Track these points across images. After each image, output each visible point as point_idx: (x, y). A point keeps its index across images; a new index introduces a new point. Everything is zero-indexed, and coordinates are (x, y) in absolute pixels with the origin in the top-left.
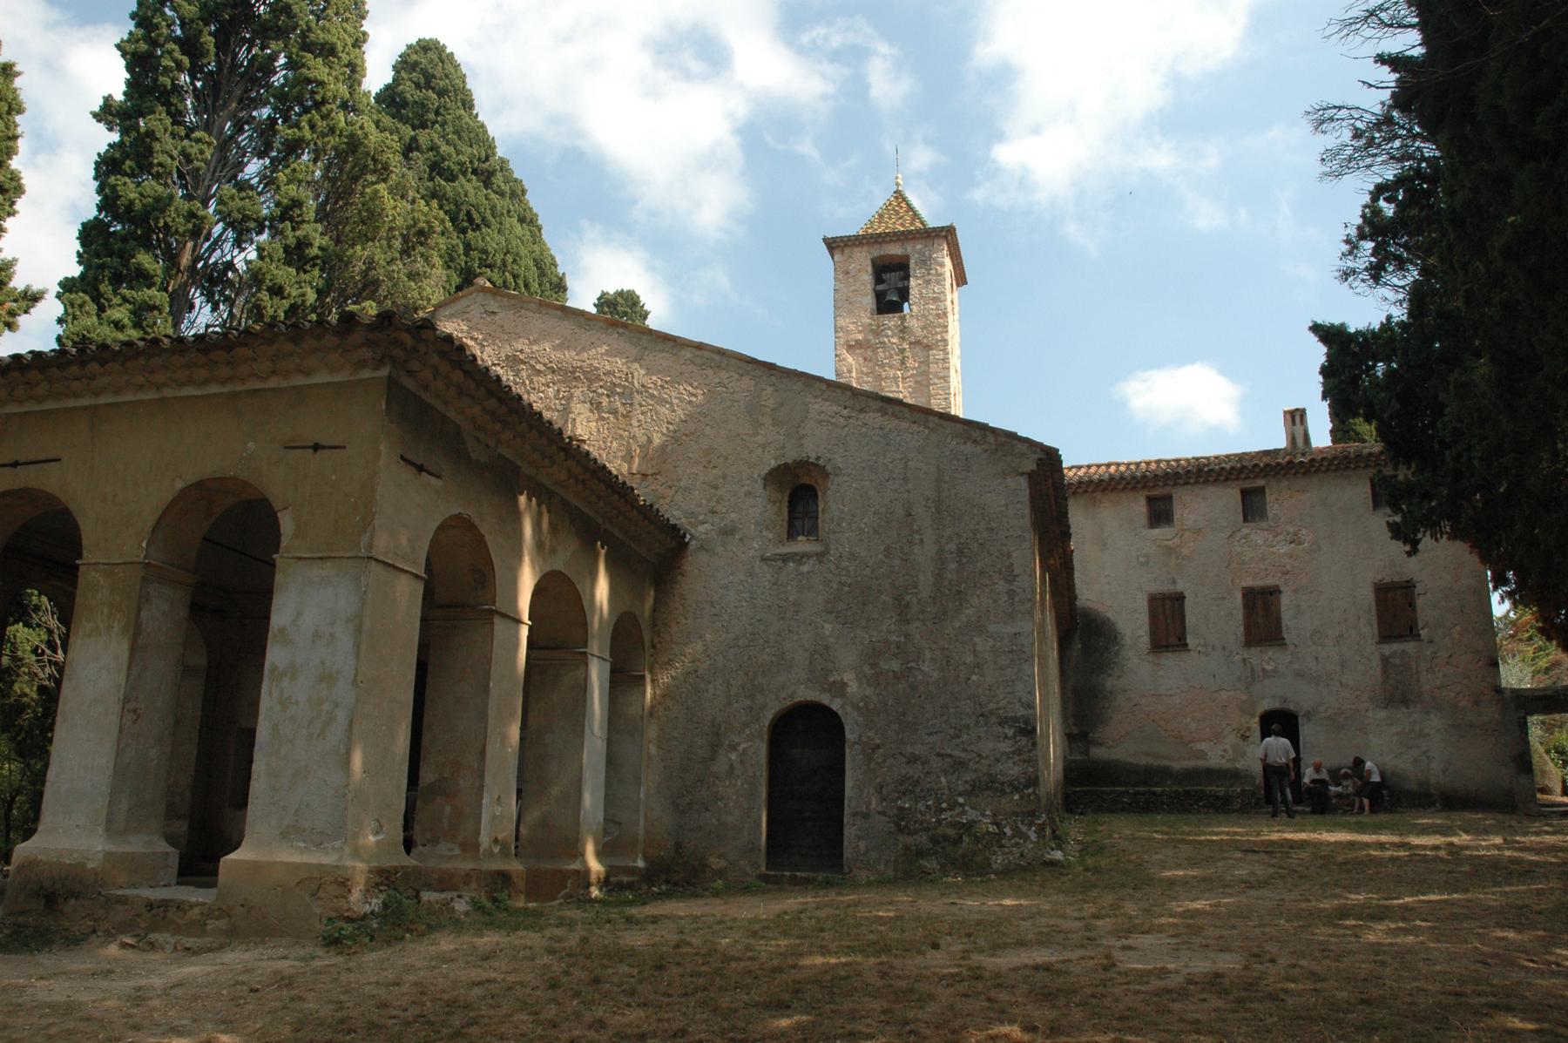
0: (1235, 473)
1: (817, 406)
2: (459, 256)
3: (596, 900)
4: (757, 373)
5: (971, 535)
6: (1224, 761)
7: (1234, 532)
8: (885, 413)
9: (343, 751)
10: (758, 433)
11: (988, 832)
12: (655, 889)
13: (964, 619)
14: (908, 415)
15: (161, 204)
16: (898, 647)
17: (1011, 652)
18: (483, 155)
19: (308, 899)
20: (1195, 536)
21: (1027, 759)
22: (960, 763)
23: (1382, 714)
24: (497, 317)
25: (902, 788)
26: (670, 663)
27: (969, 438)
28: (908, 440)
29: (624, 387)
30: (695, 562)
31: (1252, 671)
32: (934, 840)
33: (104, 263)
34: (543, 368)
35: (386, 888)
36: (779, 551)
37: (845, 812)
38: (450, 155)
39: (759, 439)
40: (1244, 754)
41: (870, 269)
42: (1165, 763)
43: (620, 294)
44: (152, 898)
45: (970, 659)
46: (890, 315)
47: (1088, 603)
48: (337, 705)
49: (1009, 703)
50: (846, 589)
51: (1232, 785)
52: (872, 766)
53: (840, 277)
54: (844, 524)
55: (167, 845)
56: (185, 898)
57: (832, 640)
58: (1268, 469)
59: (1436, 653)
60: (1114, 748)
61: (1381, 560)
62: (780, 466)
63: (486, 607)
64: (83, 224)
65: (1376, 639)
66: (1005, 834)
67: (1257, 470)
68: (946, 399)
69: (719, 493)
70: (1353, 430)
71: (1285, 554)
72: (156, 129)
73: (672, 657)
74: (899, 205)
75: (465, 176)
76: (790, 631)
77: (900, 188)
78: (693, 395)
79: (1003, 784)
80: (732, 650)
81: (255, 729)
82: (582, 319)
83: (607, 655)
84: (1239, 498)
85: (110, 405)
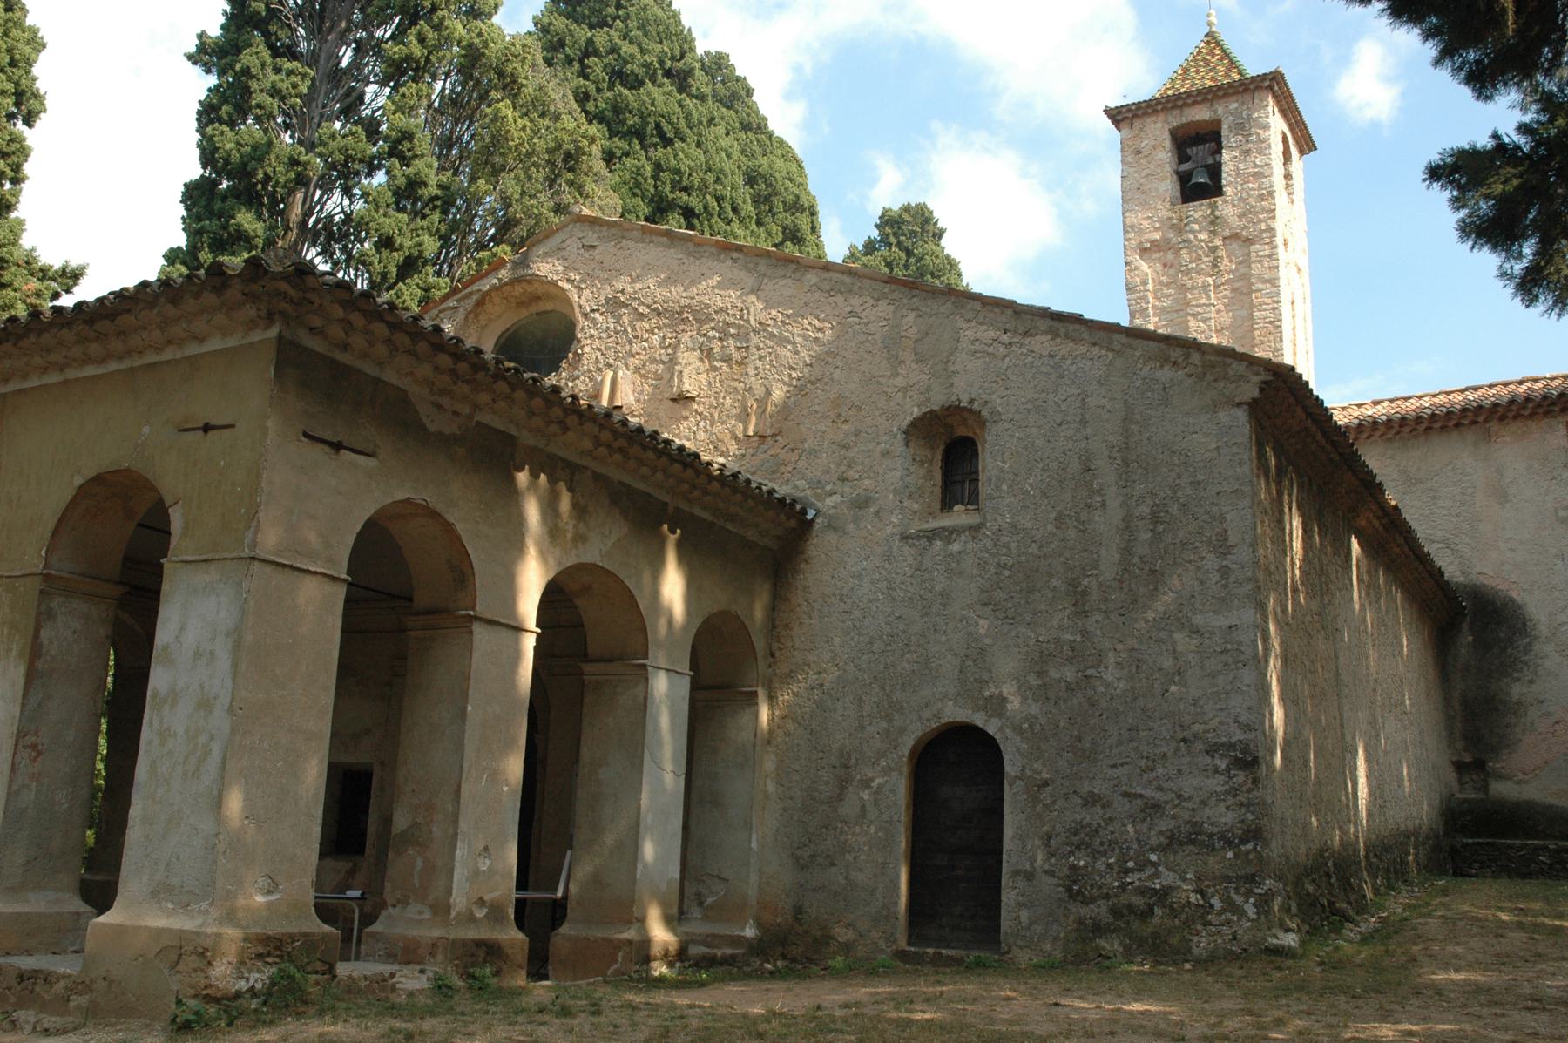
1: (969, 333)
2: (645, 180)
3: (661, 980)
4: (896, 295)
9: (215, 792)
12: (768, 966)
13: (1161, 609)
14: (1085, 335)
15: (260, 152)
16: (1073, 649)
18: (678, 52)
19: (166, 972)
21: (1246, 802)
24: (594, 253)
25: (1076, 840)
26: (790, 676)
27: (1167, 360)
28: (1087, 369)
29: (739, 327)
30: (820, 545)
32: (1116, 912)
33: (202, 227)
34: (647, 311)
35: (277, 960)
36: (926, 526)
37: (1004, 871)
38: (633, 56)
39: (899, 381)
41: (1168, 144)
43: (907, 209)
44: (23, 967)
45: (1167, 663)
47: (1481, 578)
48: (212, 738)
50: (1007, 573)
52: (1039, 808)
53: (1129, 159)
54: (1004, 487)
55: (82, 903)
56: (52, 969)
57: (988, 641)
60: (1526, 782)
62: (925, 414)
63: (464, 612)
64: (185, 185)
66: (1212, 906)
69: (851, 454)
72: (251, 65)
73: (794, 667)
75: (654, 82)
76: (935, 630)
77: (1214, 29)
78: (819, 330)
79: (1211, 836)
80: (865, 657)
82: (690, 245)
83: (685, 667)
85: (19, 392)
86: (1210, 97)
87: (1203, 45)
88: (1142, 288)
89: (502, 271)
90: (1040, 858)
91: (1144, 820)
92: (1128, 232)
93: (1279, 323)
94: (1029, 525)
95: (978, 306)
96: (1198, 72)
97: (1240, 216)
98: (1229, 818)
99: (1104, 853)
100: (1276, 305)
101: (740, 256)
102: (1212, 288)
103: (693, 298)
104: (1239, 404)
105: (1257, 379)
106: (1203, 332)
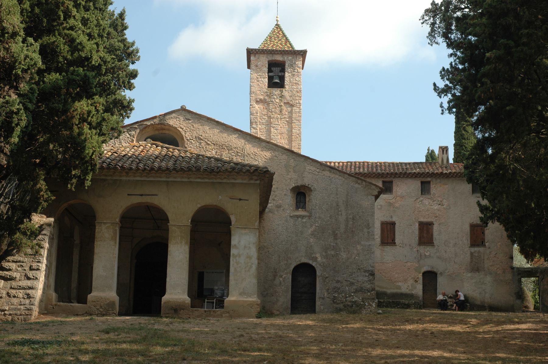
0: (419, 175)
1: (308, 167)
4: (288, 154)
5: (357, 213)
6: (407, 290)
7: (417, 199)
8: (331, 172)
10: (289, 175)
11: (361, 304)
16: (334, 247)
20: (401, 199)
22: (352, 283)
23: (469, 275)
27: (357, 182)
29: (242, 154)
31: (421, 255)
32: (345, 306)
39: (289, 176)
40: (416, 288)
42: (385, 290)
45: (355, 252)
46: (276, 89)
48: (253, 264)
49: (367, 266)
52: (325, 283)
54: (317, 207)
57: (313, 244)
58: (432, 174)
59: (491, 252)
61: (473, 215)
65: (469, 246)
67: (428, 174)
68: (299, 130)
70: (464, 146)
71: (436, 209)
77: (279, 23)
79: (365, 290)
82: (224, 126)
84: (420, 185)
86: (283, 53)
87: (275, 28)
88: (256, 114)
89: (155, 120)
91: (350, 286)
92: (252, 94)
93: (300, 135)
94: (323, 217)
95: (311, 161)
96: (275, 40)
98: (369, 286)
102: (279, 119)
103: (226, 142)
104: (373, 195)
105: (377, 190)
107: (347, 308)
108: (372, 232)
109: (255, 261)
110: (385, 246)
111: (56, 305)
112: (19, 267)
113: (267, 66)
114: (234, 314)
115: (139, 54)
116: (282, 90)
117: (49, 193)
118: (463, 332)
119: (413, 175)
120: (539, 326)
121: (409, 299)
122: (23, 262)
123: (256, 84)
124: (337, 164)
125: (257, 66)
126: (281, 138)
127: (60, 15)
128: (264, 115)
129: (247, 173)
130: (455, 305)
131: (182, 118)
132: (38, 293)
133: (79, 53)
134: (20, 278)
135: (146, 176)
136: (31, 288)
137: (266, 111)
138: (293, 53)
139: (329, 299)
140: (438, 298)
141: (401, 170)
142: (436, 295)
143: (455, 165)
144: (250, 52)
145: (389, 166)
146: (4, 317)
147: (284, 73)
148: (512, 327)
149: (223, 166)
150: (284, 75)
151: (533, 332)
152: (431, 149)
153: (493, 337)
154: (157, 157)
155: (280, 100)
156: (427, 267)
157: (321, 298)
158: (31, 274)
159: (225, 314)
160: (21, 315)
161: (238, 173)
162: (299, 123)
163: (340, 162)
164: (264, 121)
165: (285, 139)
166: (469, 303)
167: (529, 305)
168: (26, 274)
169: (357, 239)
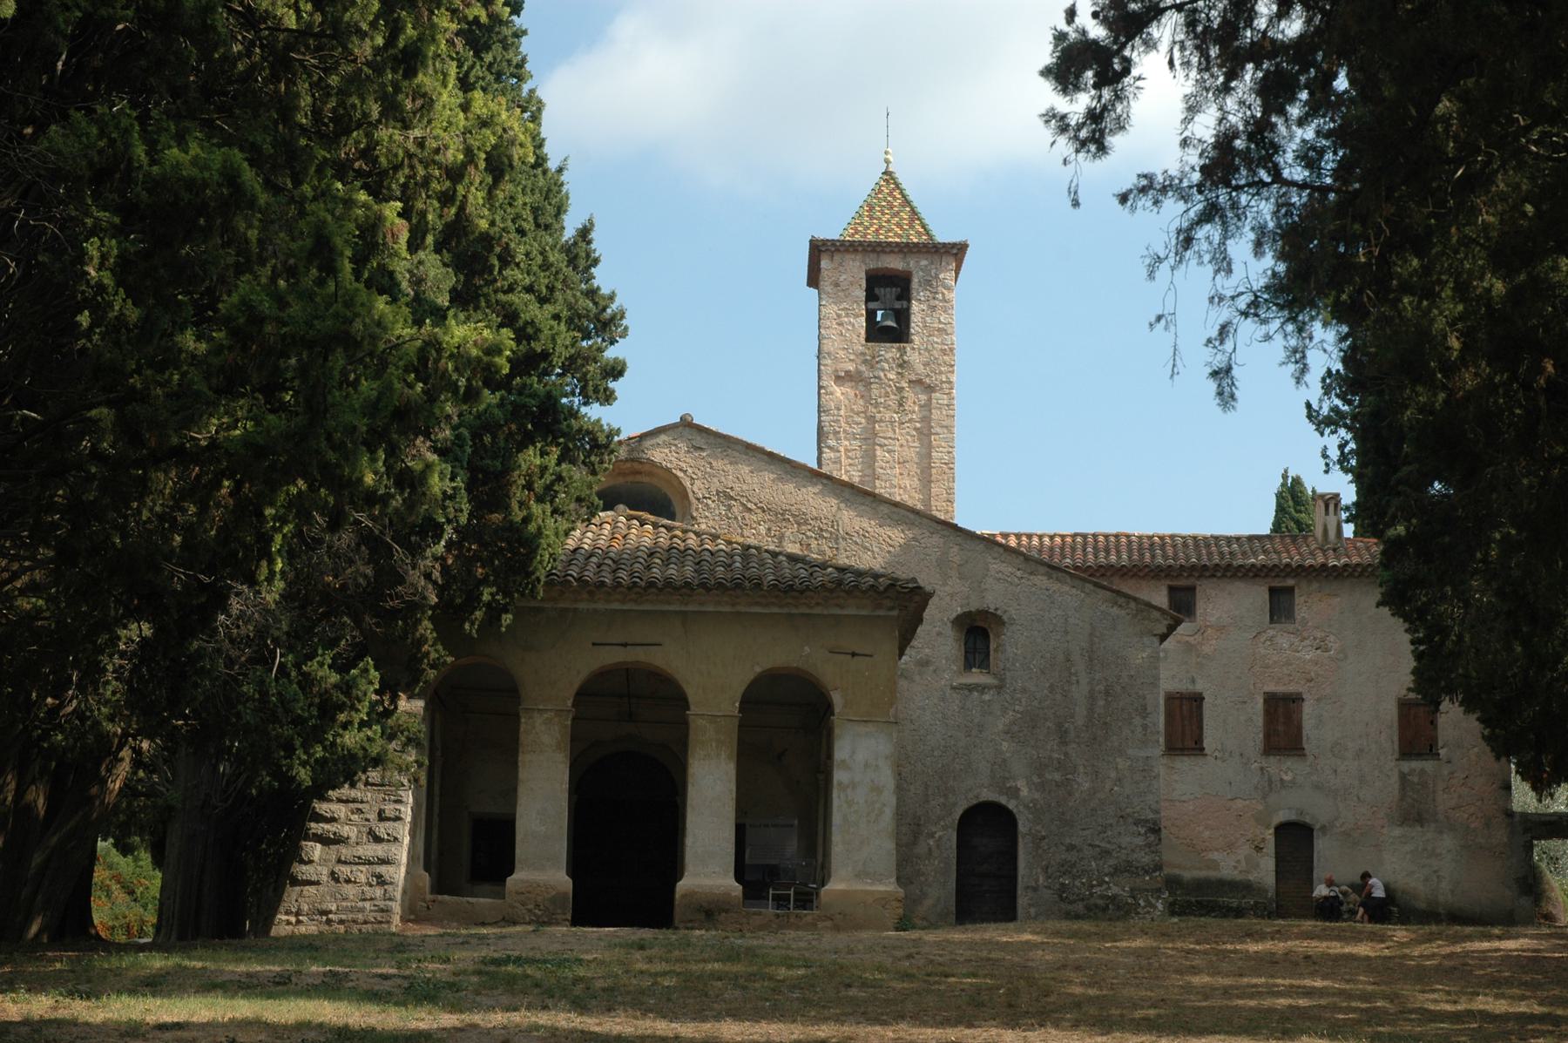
0: (1265, 570)
4: (945, 533)
6: (1236, 872)
8: (1050, 577)
11: (1127, 903)
14: (1069, 580)
17: (1144, 770)
23: (1397, 832)
27: (1116, 603)
29: (831, 533)
31: (1270, 782)
32: (1088, 908)
42: (1177, 871)
48: (884, 805)
49: (1142, 809)
51: (1244, 897)
52: (1040, 851)
59: (1452, 773)
65: (1397, 755)
67: (1289, 570)
68: (949, 452)
71: (1311, 660)
74: (890, 194)
79: (1137, 868)
81: (515, 814)
82: (787, 466)
84: (1267, 596)
86: (905, 250)
87: (882, 183)
88: (836, 412)
90: (1041, 879)
92: (824, 357)
93: (951, 466)
95: (1001, 550)
96: (883, 214)
97: (926, 365)
99: (1079, 877)
100: (951, 450)
101: (830, 483)
104: (1155, 635)
105: (1166, 622)
106: (888, 462)
107: (1095, 914)
108: (1154, 725)
109: (889, 798)
110: (1177, 758)
111: (434, 901)
112: (353, 813)
113: (864, 285)
114: (845, 920)
115: (624, 322)
116: (904, 348)
117: (440, 647)
118: (1376, 957)
119: (1249, 570)
120: (1544, 944)
121: (1240, 895)
122: (362, 802)
123: (834, 332)
124: (1047, 540)
125: (837, 285)
126: (901, 474)
127: (494, 266)
128: (858, 414)
129: (870, 593)
130: (1361, 910)
131: (683, 447)
132: (398, 874)
133: (529, 344)
134: (357, 837)
135: (635, 601)
136: (384, 862)
137: (861, 402)
138: (933, 250)
139: (1049, 891)
140: (1316, 893)
141: (1216, 559)
142: (1310, 884)
143: (1359, 544)
144: (819, 250)
145: (1185, 545)
146: (327, 927)
147: (909, 301)
148: (1486, 945)
149: (811, 574)
150: (908, 309)
151: (1530, 954)
152: (1291, 474)
153: (1440, 964)
154: (652, 554)
155: (898, 373)
156: (1287, 811)
157: (1028, 887)
158: (382, 829)
159: (824, 921)
160: (365, 922)
161: (848, 592)
162: (949, 435)
163: (1055, 535)
164: (857, 429)
165: (913, 476)
166: (1397, 906)
167: (1554, 912)
168: (370, 829)
169: (1116, 744)
